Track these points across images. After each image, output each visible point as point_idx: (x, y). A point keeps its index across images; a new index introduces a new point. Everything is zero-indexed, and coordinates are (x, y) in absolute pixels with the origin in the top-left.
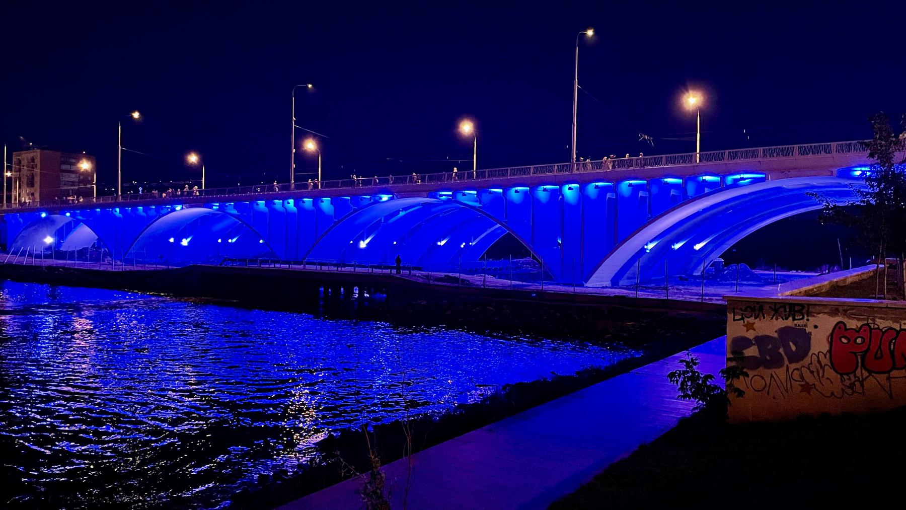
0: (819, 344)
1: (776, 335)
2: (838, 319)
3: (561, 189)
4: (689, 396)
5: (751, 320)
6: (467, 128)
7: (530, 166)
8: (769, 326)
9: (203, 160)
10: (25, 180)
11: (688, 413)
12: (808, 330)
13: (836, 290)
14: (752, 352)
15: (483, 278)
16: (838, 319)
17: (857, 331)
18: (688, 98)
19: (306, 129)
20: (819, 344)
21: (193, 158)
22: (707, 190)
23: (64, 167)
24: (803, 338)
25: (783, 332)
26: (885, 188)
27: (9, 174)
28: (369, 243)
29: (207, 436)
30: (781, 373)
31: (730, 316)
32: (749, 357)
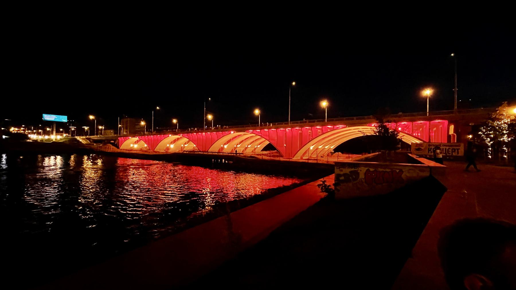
0: (362, 176)
1: (349, 173)
2: (367, 168)
3: (285, 130)
4: (324, 192)
5: (342, 169)
6: (257, 112)
7: (314, 120)
8: (347, 171)
9: (179, 122)
10: (125, 127)
11: (323, 197)
12: (359, 171)
13: (367, 159)
14: (342, 178)
15: (339, 160)
16: (367, 168)
17: (373, 172)
18: (326, 102)
19: (209, 111)
20: (362, 176)
21: (175, 121)
22: (329, 130)
23: (136, 124)
24: (357, 174)
25: (351, 172)
26: (381, 130)
27: (120, 126)
28: (313, 147)
29: (4, 156)
30: (350, 184)
31: (336, 168)
32: (341, 180)
